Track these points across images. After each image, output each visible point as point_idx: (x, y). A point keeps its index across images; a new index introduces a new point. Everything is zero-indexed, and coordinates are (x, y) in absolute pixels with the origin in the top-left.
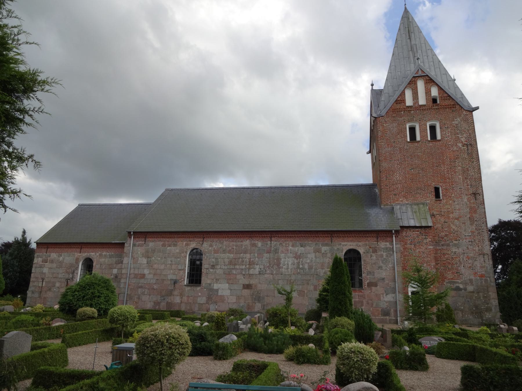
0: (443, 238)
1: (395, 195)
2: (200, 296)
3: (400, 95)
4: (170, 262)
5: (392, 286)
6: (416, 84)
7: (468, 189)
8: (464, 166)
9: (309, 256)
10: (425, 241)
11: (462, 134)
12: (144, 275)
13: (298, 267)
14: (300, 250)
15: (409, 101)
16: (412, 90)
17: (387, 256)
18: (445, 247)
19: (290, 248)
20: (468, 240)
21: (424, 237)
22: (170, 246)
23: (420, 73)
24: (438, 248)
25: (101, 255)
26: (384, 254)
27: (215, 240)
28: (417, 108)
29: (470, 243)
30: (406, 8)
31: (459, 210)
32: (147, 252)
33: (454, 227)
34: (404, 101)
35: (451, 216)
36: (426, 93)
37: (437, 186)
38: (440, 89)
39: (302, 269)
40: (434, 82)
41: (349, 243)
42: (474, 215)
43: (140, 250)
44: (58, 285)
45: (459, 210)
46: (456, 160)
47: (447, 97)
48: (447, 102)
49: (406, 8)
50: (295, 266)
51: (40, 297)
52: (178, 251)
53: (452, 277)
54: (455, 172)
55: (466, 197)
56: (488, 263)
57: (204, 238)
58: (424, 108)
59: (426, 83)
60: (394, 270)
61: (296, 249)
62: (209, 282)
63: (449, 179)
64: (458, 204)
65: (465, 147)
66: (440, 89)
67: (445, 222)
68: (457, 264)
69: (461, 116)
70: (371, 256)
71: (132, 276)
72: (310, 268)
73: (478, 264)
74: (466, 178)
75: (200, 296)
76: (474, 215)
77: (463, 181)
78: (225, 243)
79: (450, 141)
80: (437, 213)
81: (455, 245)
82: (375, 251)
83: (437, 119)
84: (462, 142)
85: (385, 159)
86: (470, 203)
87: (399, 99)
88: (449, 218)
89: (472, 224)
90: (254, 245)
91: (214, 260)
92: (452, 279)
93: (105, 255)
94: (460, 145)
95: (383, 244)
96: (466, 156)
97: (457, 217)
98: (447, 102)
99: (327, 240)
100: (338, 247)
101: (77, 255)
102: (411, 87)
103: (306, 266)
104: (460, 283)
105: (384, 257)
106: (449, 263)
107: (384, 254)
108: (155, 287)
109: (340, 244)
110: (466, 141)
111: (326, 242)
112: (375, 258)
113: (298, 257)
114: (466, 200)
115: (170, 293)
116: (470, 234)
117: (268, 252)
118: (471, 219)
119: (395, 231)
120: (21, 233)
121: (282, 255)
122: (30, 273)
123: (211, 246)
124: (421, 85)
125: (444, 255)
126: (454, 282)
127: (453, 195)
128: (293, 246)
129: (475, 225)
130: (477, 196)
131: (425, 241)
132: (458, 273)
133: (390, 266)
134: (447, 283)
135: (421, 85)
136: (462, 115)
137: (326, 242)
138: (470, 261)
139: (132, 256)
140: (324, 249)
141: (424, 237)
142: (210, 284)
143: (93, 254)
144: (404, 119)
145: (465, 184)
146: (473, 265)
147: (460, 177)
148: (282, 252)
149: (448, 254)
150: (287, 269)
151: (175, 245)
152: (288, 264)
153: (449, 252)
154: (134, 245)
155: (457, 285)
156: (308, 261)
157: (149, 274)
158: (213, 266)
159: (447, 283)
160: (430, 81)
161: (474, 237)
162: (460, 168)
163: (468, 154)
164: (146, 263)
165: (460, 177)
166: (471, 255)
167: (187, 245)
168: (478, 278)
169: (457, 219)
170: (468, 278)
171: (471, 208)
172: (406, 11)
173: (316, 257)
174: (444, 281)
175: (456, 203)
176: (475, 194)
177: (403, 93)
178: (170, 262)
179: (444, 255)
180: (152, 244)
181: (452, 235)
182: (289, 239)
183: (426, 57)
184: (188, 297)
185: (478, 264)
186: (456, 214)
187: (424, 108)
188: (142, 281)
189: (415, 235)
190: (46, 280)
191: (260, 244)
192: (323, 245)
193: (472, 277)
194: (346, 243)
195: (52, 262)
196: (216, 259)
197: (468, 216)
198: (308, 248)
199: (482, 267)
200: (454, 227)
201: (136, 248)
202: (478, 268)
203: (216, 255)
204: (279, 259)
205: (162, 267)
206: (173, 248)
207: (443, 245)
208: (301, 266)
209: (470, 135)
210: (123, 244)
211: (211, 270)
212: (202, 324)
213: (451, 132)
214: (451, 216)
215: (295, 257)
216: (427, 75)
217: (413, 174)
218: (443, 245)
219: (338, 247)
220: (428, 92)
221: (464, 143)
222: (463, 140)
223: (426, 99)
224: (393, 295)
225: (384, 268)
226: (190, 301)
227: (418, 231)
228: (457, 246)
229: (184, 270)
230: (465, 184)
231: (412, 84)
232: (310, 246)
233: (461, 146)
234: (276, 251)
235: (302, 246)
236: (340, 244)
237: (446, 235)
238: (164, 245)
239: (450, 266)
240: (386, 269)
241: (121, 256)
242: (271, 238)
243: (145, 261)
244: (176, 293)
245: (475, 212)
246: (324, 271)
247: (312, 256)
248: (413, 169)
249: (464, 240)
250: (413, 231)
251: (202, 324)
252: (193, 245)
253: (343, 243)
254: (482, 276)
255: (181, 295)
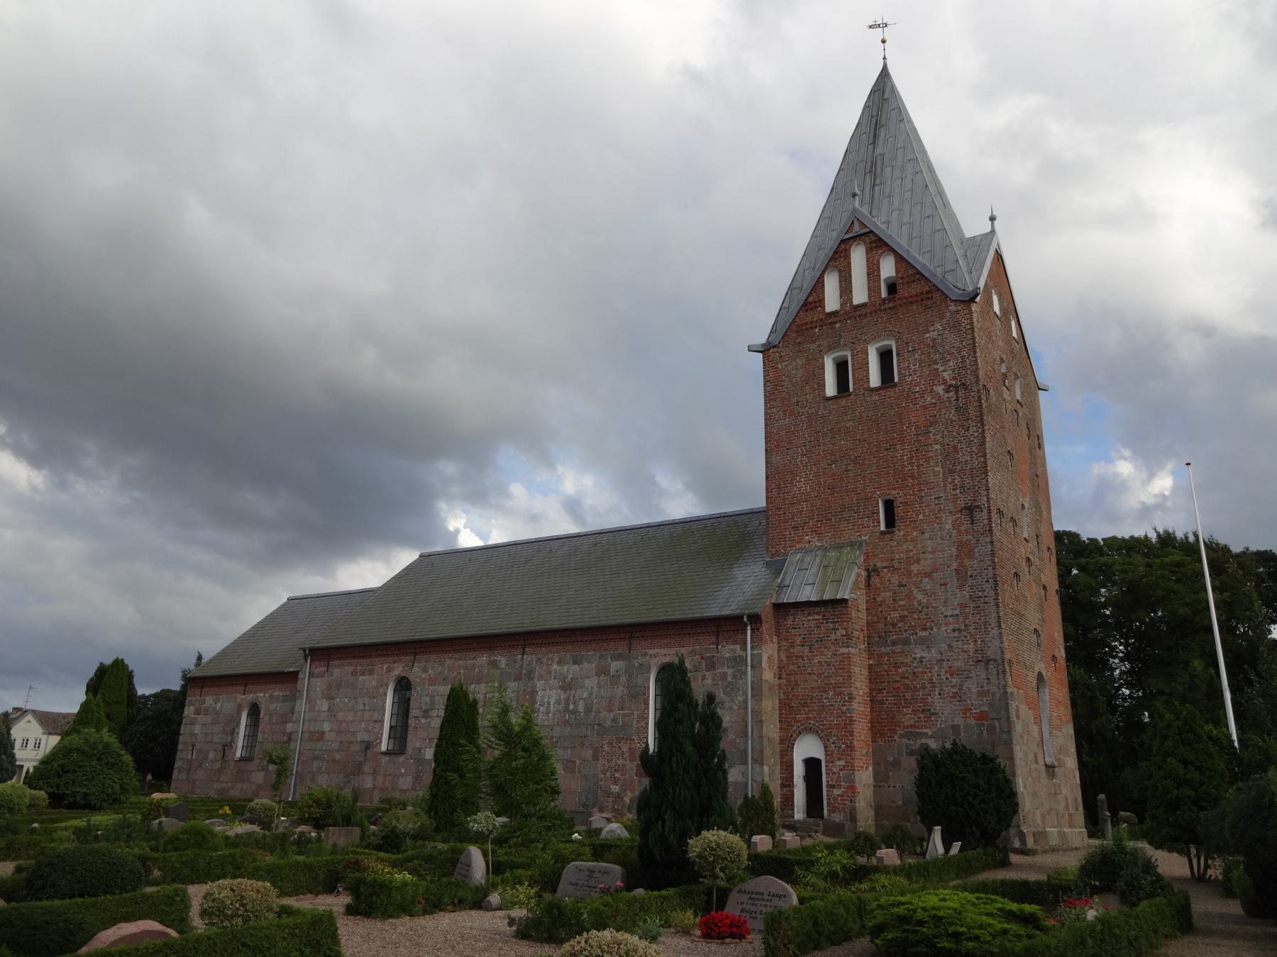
0: (894, 625)
1: (795, 528)
2: (402, 775)
3: (814, 289)
4: (361, 707)
5: (742, 747)
6: (847, 257)
7: (955, 498)
8: (946, 441)
9: (587, 683)
10: (833, 637)
11: (945, 362)
12: (323, 733)
13: (567, 710)
14: (571, 670)
15: (832, 302)
16: (840, 272)
17: (734, 677)
18: (898, 648)
19: (555, 667)
20: (951, 627)
21: (831, 626)
22: (363, 674)
23: (857, 229)
24: (883, 649)
25: (271, 696)
26: (730, 672)
27: (433, 657)
28: (851, 313)
29: (956, 634)
30: (885, 68)
31: (933, 552)
32: (329, 687)
33: (920, 597)
34: (821, 302)
35: (915, 568)
36: (869, 274)
37: (889, 497)
38: (900, 260)
39: (575, 712)
40: (887, 244)
41: (663, 651)
42: (967, 562)
43: (319, 684)
44: (211, 755)
45: (933, 552)
46: (931, 429)
47: (914, 275)
48: (914, 289)
49: (885, 68)
50: (561, 707)
51: (188, 779)
52: (374, 683)
53: (912, 722)
54: (927, 460)
55: (951, 519)
56: (995, 682)
57: (415, 654)
58: (864, 311)
59: (869, 251)
60: (746, 708)
61: (565, 668)
62: (418, 745)
63: (913, 477)
64: (931, 538)
65: (951, 394)
66: (900, 260)
67: (901, 585)
68: (924, 688)
69: (943, 317)
70: (704, 678)
71: (306, 736)
72: (588, 709)
73: (972, 686)
74: (951, 471)
75: (402, 775)
76: (967, 562)
77: (945, 479)
78: (448, 662)
79: (918, 384)
80: (885, 564)
81: (923, 641)
82: (711, 666)
83: (891, 334)
84: (945, 382)
85: (777, 446)
86: (959, 532)
87: (811, 299)
88: (909, 573)
89: (961, 587)
90: (494, 664)
91: (427, 699)
92: (912, 726)
93: (278, 697)
94: (940, 389)
95: (728, 650)
96: (953, 415)
97: (928, 569)
98: (914, 289)
99: (622, 648)
100: (641, 660)
101: (240, 697)
102: (836, 267)
103: (581, 707)
104: (931, 737)
105: (729, 679)
106: (908, 688)
107: (730, 672)
108: (338, 757)
109: (646, 654)
110: (955, 379)
111: (620, 651)
112: (710, 681)
113: (566, 686)
114: (949, 526)
115: (358, 770)
116: (957, 612)
117: (517, 679)
118: (961, 573)
119: (750, 617)
120: (194, 660)
121: (540, 684)
122: (178, 734)
123: (425, 670)
124: (858, 257)
125: (896, 666)
126: (917, 734)
127: (921, 517)
128: (559, 663)
129: (968, 588)
130: (977, 515)
131: (833, 637)
132: (928, 712)
133: (740, 699)
134: (902, 736)
135: (858, 257)
136: (948, 314)
137: (620, 651)
138: (954, 681)
139: (308, 697)
140: (615, 666)
141: (831, 626)
142: (419, 750)
143: (261, 696)
144: (820, 346)
145: (950, 486)
146: (961, 689)
147: (937, 469)
148: (541, 677)
149: (906, 665)
150: (548, 713)
151: (371, 672)
152: (549, 703)
153: (908, 660)
154: (311, 675)
155: (924, 741)
156: (585, 695)
157: (330, 731)
158: (426, 711)
159: (902, 736)
160: (877, 244)
161: (966, 617)
162: (938, 447)
163: (958, 409)
164: (326, 708)
165: (937, 469)
166: (958, 664)
167: (389, 670)
168: (974, 722)
169: (928, 575)
170: (950, 722)
171: (961, 545)
172: (884, 74)
173: (599, 686)
174: (894, 731)
175: (927, 535)
176: (970, 510)
177: (819, 285)
178: (361, 707)
179: (896, 666)
180: (340, 671)
181: (915, 616)
182: (554, 649)
183: (899, 182)
184: (385, 775)
185: (972, 686)
186: (926, 565)
187: (864, 311)
188: (319, 745)
189: (813, 624)
190: (198, 747)
191: (503, 662)
192: (614, 658)
193: (959, 720)
194: (656, 651)
195: (206, 712)
196: (433, 697)
197: (955, 565)
198: (586, 665)
199: (982, 694)
200: (920, 597)
201: (313, 680)
202: (974, 697)
203: (431, 688)
204: (533, 693)
205: (350, 717)
206: (367, 677)
207: (894, 643)
208: (571, 707)
209: (963, 361)
210: (292, 677)
211: (423, 721)
212: (88, 821)
213: (921, 361)
214: (915, 568)
215: (562, 688)
216: (872, 232)
217: (834, 475)
218: (894, 643)
219: (641, 660)
220: (873, 272)
221: (949, 382)
222: (947, 377)
223: (869, 288)
224: (743, 768)
225: (727, 705)
226: (388, 785)
227: (818, 613)
228: (926, 643)
229: (382, 721)
230: (950, 486)
231: (838, 258)
232: (589, 662)
233: (942, 393)
234: (530, 676)
235: (575, 663)
236: (646, 654)
237: (902, 618)
238: (354, 673)
239: (908, 695)
240: (731, 708)
241: (293, 698)
242: (524, 647)
243: (324, 705)
244: (367, 768)
245: (970, 555)
246: (612, 715)
247: (591, 683)
248: (834, 462)
249: (943, 628)
250: (809, 614)
251: (88, 821)
252: (398, 670)
253: (651, 652)
254: (982, 717)
255: (375, 772)
